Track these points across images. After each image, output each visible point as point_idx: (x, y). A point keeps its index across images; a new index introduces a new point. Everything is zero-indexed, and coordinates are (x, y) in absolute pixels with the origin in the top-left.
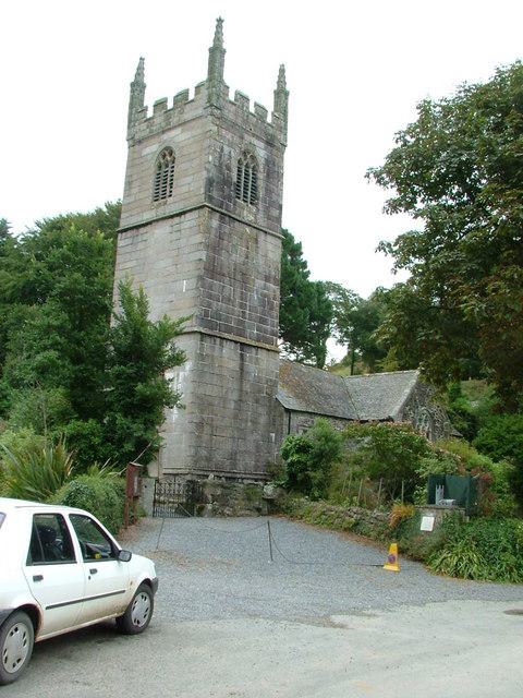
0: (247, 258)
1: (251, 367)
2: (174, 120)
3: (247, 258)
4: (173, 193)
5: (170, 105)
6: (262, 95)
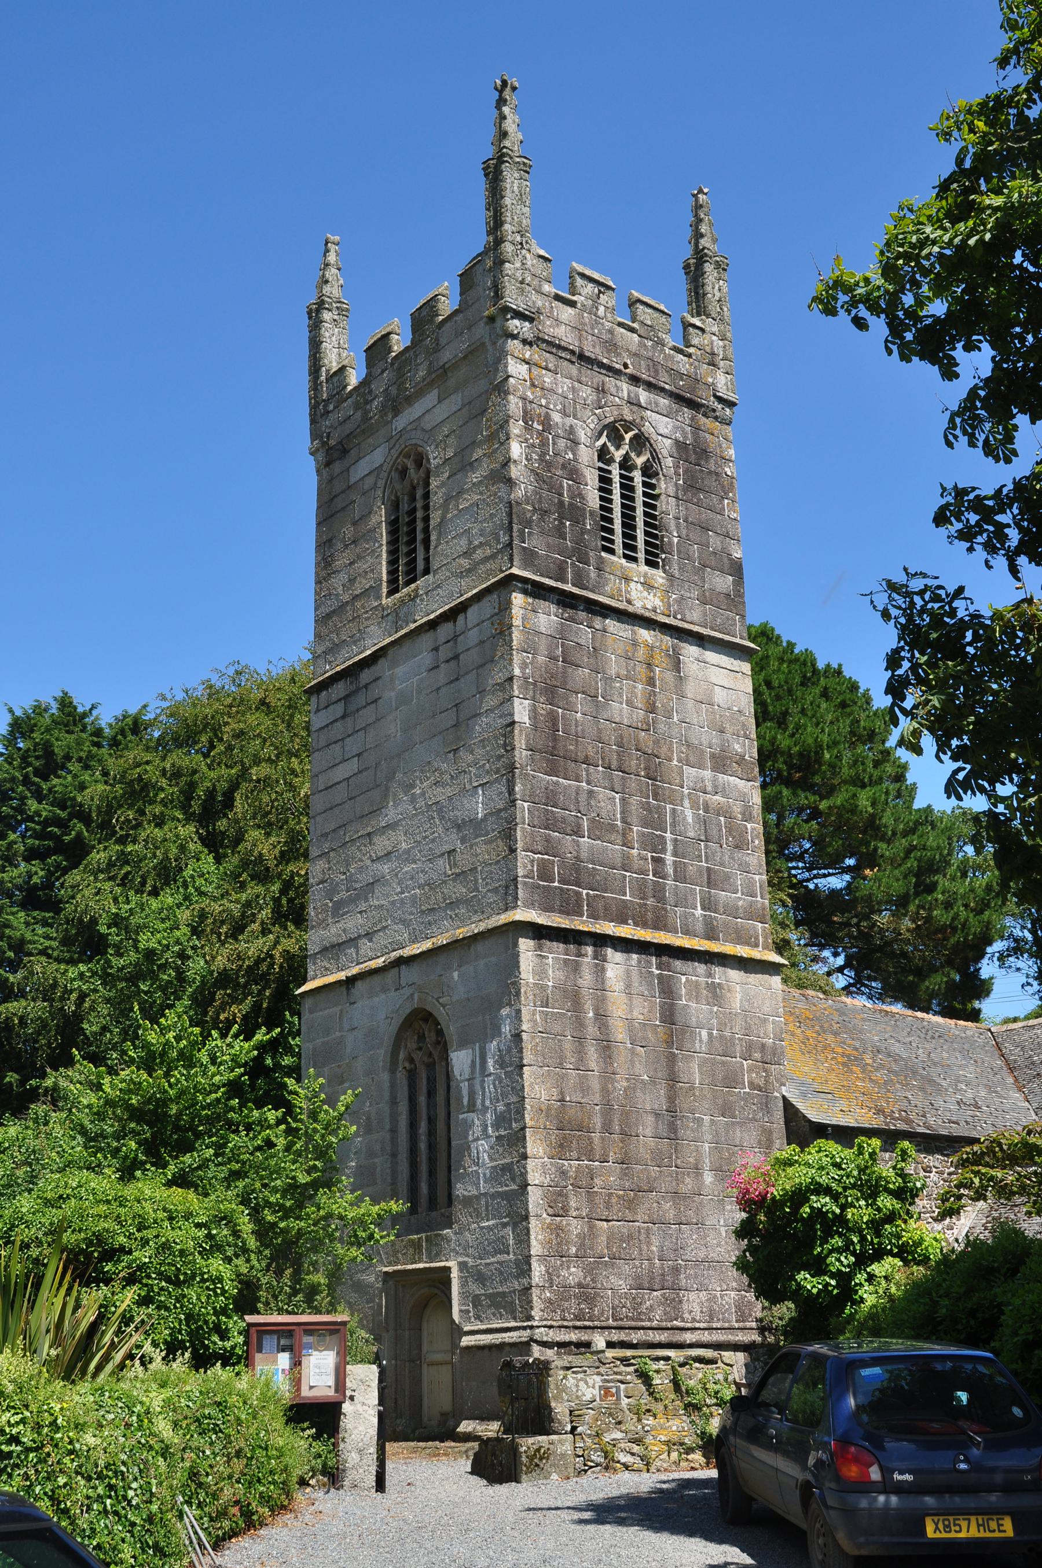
0: (651, 709)
1: (695, 1010)
3: (651, 709)
4: (435, 565)
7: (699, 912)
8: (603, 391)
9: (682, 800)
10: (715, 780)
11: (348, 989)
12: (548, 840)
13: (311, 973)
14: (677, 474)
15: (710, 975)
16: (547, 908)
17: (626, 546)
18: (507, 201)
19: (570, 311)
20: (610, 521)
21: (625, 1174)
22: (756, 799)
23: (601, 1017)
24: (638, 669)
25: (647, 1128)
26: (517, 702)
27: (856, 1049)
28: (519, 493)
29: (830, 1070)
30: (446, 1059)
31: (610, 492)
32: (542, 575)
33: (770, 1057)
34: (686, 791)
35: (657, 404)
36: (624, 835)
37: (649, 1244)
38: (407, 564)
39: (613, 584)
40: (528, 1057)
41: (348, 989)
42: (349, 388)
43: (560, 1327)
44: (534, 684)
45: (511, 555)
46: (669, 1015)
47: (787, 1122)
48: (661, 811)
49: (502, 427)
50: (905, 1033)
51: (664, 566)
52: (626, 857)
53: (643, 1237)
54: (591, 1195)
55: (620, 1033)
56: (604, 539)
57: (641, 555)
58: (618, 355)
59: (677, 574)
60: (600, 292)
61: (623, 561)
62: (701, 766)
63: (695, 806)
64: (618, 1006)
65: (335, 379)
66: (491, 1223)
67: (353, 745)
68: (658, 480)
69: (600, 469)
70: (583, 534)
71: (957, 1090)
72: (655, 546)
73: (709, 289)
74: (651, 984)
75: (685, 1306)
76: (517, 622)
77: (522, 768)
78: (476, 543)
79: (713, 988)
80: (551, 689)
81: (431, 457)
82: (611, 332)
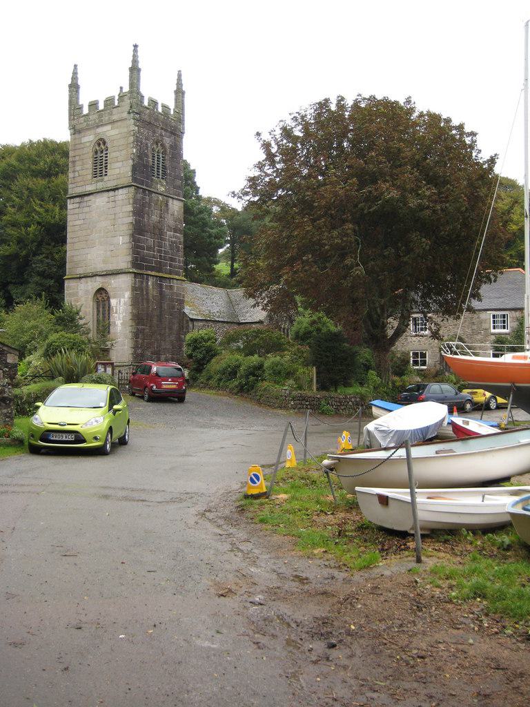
2: (105, 118)
3: (161, 217)
5: (101, 107)
6: (166, 99)
23: (147, 293)
25: (155, 321)
54: (144, 334)
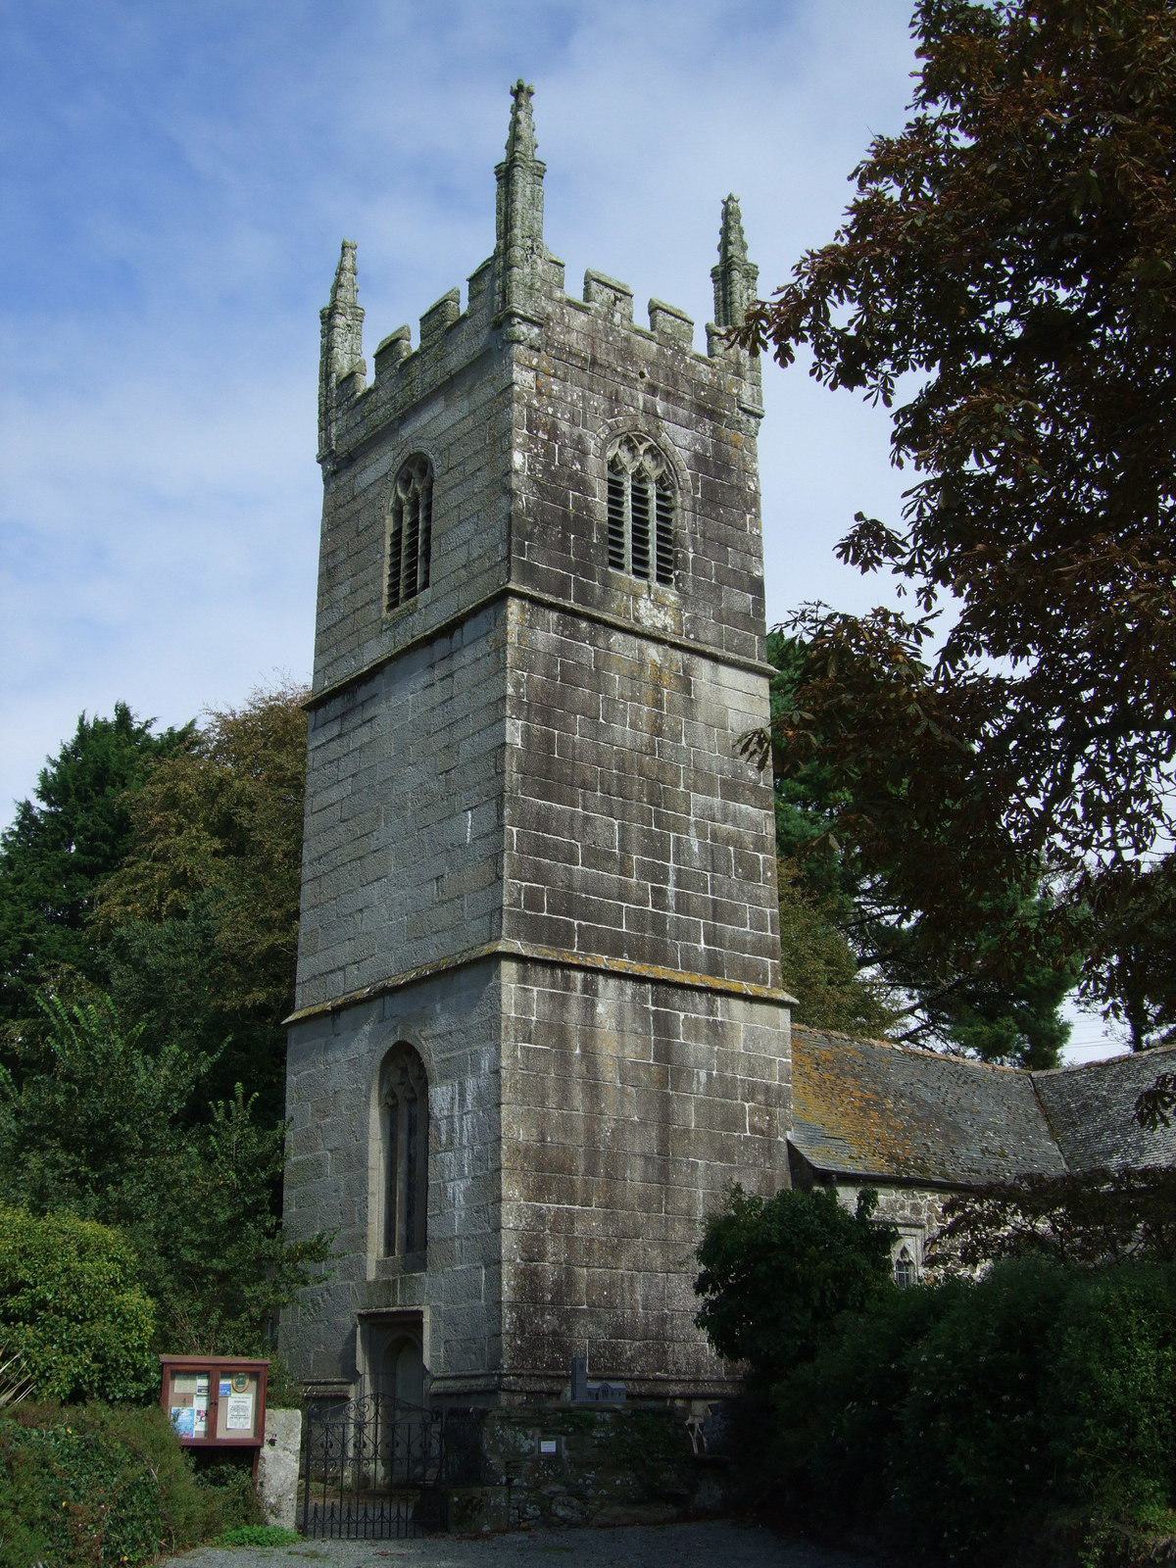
0: (657, 731)
1: (694, 1048)
3: (657, 731)
4: (433, 578)
7: (703, 945)
8: (617, 400)
9: (688, 828)
10: (725, 808)
11: (334, 1020)
12: (538, 867)
13: (298, 1002)
14: (696, 488)
15: (711, 1012)
16: (533, 938)
17: (635, 561)
18: (518, 205)
19: (583, 317)
20: (621, 535)
21: (608, 1219)
22: (770, 830)
23: (590, 1055)
24: (644, 690)
26: (508, 723)
27: (877, 1094)
28: (521, 504)
29: (844, 1115)
30: (425, 1093)
31: (620, 504)
32: (542, 590)
33: (773, 1098)
34: (692, 819)
35: (675, 415)
36: (622, 863)
37: (632, 1292)
38: (407, 577)
39: (620, 600)
40: (507, 1095)
41: (334, 1020)
42: (359, 394)
43: (530, 1376)
44: (529, 705)
45: (509, 569)
46: (664, 1052)
47: (792, 1168)
48: (663, 840)
49: (504, 434)
50: (935, 1077)
51: (677, 583)
52: (623, 886)
53: (626, 1285)
54: (570, 1241)
55: (610, 1074)
56: (611, 553)
57: (653, 571)
58: (634, 363)
59: (691, 591)
60: (616, 298)
61: (633, 577)
62: (710, 792)
63: (702, 834)
64: (608, 1047)
65: (345, 385)
66: (464, 1267)
67: (349, 766)
68: (674, 493)
69: (610, 481)
70: (588, 548)
71: (984, 1137)
72: (668, 562)
73: (736, 297)
74: (646, 1021)
75: (670, 1358)
76: (512, 638)
77: (511, 791)
78: (475, 555)
79: (714, 1026)
80: (545, 708)
81: (435, 465)
82: (627, 339)
